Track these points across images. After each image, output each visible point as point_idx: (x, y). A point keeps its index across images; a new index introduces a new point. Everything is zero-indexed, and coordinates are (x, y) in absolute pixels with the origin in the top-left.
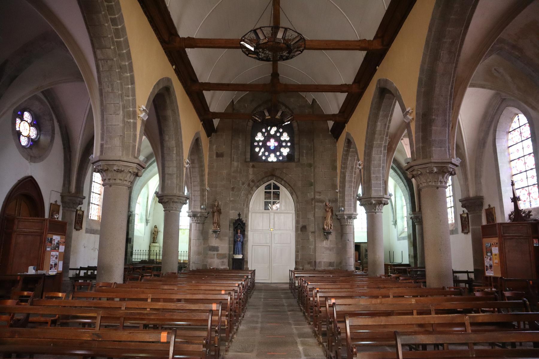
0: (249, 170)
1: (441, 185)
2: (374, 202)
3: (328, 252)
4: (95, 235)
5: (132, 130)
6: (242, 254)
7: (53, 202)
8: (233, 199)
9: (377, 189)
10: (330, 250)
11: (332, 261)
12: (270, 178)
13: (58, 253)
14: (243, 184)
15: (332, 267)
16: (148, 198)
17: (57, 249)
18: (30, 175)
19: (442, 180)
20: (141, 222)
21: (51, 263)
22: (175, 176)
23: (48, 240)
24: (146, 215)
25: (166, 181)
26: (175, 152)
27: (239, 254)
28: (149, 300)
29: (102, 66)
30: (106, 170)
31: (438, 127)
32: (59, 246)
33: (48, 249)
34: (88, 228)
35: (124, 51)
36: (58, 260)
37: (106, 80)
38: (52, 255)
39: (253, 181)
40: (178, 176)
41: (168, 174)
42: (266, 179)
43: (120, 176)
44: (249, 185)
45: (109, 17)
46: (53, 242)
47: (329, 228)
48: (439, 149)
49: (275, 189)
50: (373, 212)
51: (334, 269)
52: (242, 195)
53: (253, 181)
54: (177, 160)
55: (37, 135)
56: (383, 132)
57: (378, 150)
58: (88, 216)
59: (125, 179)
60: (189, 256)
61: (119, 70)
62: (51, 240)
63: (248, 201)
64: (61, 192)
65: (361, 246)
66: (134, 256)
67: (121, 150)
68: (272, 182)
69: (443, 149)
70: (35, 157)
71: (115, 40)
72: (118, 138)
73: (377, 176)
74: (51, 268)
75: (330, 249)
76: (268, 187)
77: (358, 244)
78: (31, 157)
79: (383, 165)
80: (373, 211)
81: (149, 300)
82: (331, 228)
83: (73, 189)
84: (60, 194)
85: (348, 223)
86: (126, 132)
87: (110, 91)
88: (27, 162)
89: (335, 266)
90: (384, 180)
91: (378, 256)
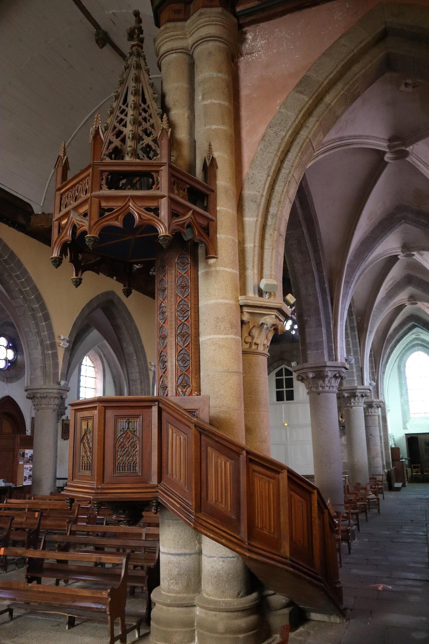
1: (323, 390)
2: (346, 395)
5: (51, 360)
12: (280, 362)
17: (30, 462)
18: (8, 395)
19: (323, 385)
21: (25, 475)
22: (138, 382)
23: (20, 454)
25: (131, 387)
26: (135, 358)
28: (26, 510)
29: (19, 312)
30: (32, 398)
31: (311, 328)
33: (21, 463)
35: (33, 297)
37: (24, 322)
38: (25, 468)
40: (143, 381)
41: (132, 380)
43: (44, 401)
45: (13, 274)
46: (26, 456)
48: (315, 351)
50: (349, 407)
54: (139, 365)
55: (15, 355)
59: (50, 403)
61: (32, 312)
65: (419, 439)
68: (284, 366)
69: (320, 351)
70: (11, 378)
71: (23, 290)
72: (39, 369)
74: (25, 480)
77: (414, 436)
78: (7, 378)
79: (355, 349)
80: (348, 405)
81: (26, 510)
85: (369, 413)
86: (47, 363)
87: (29, 331)
88: (3, 384)
90: (359, 366)
91: (356, 460)
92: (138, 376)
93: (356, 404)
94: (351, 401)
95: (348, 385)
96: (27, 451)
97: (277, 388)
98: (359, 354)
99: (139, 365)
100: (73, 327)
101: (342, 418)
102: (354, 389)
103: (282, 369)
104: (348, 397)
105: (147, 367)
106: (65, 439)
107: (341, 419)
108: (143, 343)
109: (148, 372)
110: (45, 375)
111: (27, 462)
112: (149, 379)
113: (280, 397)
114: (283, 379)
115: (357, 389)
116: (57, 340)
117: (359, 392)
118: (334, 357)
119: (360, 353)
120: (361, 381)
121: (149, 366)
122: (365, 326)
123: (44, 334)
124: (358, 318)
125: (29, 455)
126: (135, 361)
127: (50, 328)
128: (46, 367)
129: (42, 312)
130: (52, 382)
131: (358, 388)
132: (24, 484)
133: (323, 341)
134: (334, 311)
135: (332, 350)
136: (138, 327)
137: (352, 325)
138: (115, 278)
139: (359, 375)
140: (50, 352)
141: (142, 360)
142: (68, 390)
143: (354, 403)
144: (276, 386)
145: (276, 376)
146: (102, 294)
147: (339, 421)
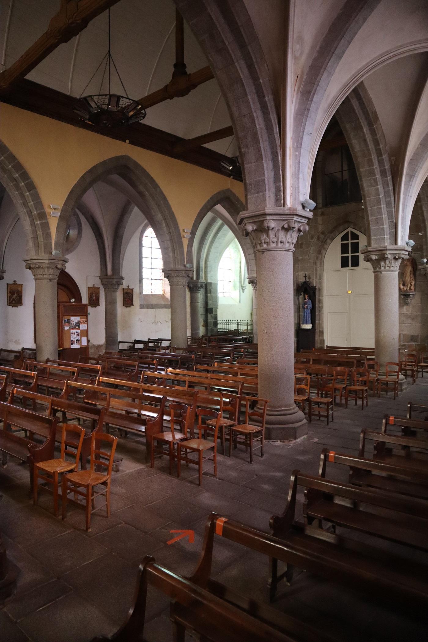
0: (317, 219)
3: (409, 321)
4: (155, 309)
6: (312, 323)
7: (92, 286)
8: (302, 257)
9: (378, 237)
10: (413, 319)
11: (415, 334)
13: (79, 331)
14: (312, 237)
15: (414, 342)
16: (241, 263)
17: (77, 327)
20: (235, 290)
21: (72, 339)
23: (65, 321)
24: (240, 282)
26: (164, 225)
27: (306, 324)
31: (251, 163)
32: (79, 325)
33: (66, 329)
34: (142, 303)
36: (80, 336)
39: (323, 233)
42: (341, 228)
44: (318, 238)
46: (71, 322)
47: (408, 288)
49: (343, 241)
51: (418, 345)
52: (311, 252)
53: (323, 233)
56: (366, 152)
57: (370, 179)
58: (141, 293)
59: (44, 273)
60: (252, 325)
62: (69, 321)
63: (321, 258)
64: (162, 268)
66: (219, 327)
67: (34, 249)
68: (350, 230)
69: (261, 194)
73: (377, 218)
74: (72, 344)
75: (413, 318)
76: (345, 238)
79: (388, 199)
82: (410, 289)
83: (109, 272)
84: (99, 278)
89: (419, 341)
90: (393, 222)
92: (170, 244)
93: (387, 268)
94: (380, 265)
95: (376, 246)
96: (72, 318)
97: (341, 254)
98: (393, 206)
99: (170, 232)
100: (69, 196)
101: (404, 285)
102: (384, 250)
103: (348, 232)
104: (376, 259)
105: (180, 234)
106: (127, 307)
107: (402, 287)
108: (173, 209)
109: (181, 239)
110: (37, 246)
111: (74, 328)
112: (182, 246)
113: (344, 263)
114: (348, 243)
115: (387, 250)
116: (47, 210)
117: (390, 254)
118: (282, 201)
119: (395, 203)
120: (394, 238)
121: (182, 233)
122: (400, 168)
123: (30, 204)
124: (392, 158)
125: (75, 321)
126: (165, 229)
127: (36, 198)
128: (37, 238)
129: (23, 182)
130: (43, 252)
131: (388, 248)
132: (72, 347)
133: (265, 180)
134: (281, 136)
135: (280, 191)
136: (165, 193)
137: (382, 168)
138: (127, 141)
139: (392, 232)
140: (39, 222)
141: (173, 227)
142: (67, 261)
143: (385, 267)
144: (342, 251)
145: (342, 241)
146: (111, 159)
147: (400, 289)
